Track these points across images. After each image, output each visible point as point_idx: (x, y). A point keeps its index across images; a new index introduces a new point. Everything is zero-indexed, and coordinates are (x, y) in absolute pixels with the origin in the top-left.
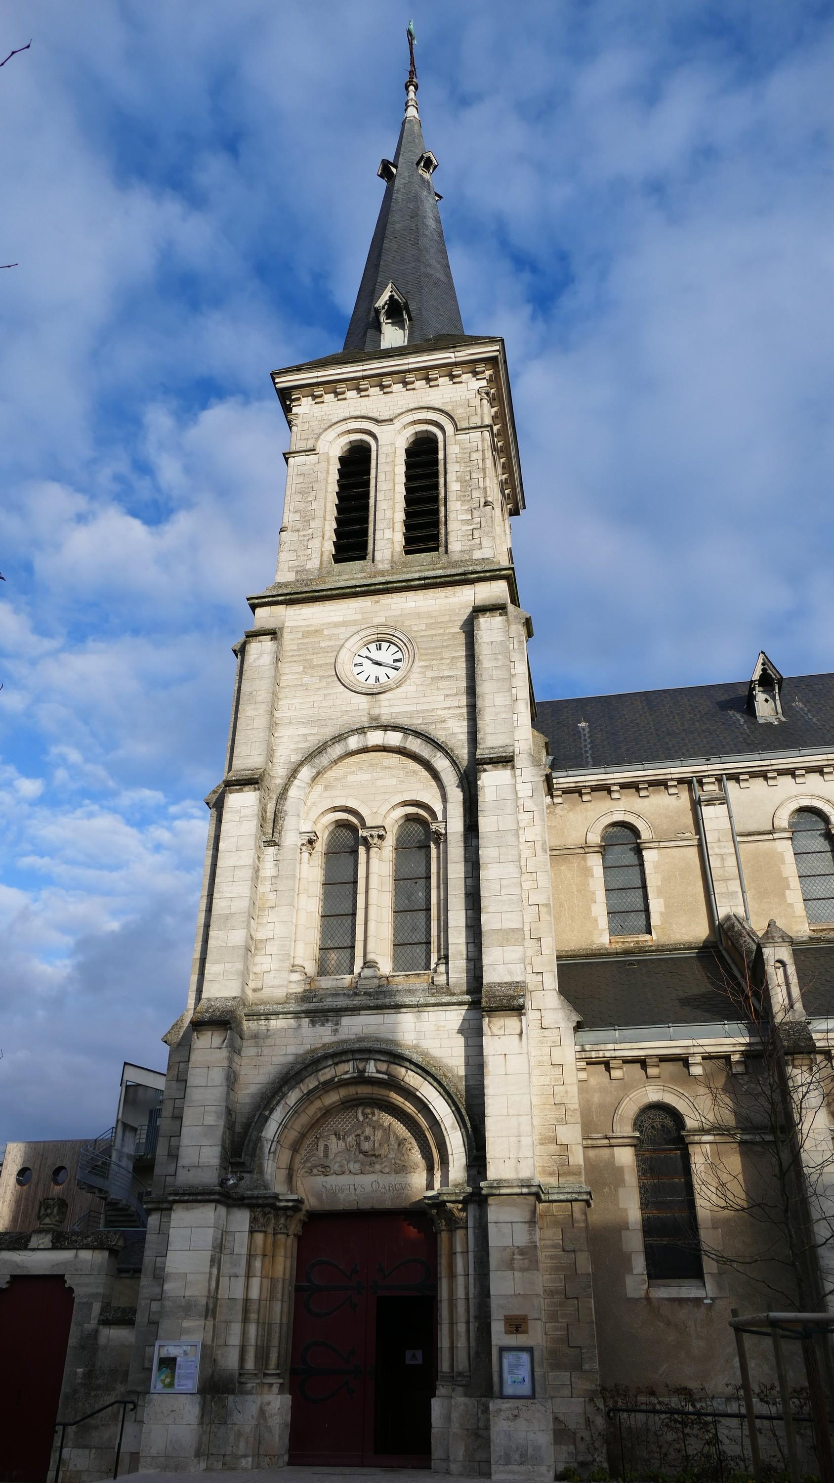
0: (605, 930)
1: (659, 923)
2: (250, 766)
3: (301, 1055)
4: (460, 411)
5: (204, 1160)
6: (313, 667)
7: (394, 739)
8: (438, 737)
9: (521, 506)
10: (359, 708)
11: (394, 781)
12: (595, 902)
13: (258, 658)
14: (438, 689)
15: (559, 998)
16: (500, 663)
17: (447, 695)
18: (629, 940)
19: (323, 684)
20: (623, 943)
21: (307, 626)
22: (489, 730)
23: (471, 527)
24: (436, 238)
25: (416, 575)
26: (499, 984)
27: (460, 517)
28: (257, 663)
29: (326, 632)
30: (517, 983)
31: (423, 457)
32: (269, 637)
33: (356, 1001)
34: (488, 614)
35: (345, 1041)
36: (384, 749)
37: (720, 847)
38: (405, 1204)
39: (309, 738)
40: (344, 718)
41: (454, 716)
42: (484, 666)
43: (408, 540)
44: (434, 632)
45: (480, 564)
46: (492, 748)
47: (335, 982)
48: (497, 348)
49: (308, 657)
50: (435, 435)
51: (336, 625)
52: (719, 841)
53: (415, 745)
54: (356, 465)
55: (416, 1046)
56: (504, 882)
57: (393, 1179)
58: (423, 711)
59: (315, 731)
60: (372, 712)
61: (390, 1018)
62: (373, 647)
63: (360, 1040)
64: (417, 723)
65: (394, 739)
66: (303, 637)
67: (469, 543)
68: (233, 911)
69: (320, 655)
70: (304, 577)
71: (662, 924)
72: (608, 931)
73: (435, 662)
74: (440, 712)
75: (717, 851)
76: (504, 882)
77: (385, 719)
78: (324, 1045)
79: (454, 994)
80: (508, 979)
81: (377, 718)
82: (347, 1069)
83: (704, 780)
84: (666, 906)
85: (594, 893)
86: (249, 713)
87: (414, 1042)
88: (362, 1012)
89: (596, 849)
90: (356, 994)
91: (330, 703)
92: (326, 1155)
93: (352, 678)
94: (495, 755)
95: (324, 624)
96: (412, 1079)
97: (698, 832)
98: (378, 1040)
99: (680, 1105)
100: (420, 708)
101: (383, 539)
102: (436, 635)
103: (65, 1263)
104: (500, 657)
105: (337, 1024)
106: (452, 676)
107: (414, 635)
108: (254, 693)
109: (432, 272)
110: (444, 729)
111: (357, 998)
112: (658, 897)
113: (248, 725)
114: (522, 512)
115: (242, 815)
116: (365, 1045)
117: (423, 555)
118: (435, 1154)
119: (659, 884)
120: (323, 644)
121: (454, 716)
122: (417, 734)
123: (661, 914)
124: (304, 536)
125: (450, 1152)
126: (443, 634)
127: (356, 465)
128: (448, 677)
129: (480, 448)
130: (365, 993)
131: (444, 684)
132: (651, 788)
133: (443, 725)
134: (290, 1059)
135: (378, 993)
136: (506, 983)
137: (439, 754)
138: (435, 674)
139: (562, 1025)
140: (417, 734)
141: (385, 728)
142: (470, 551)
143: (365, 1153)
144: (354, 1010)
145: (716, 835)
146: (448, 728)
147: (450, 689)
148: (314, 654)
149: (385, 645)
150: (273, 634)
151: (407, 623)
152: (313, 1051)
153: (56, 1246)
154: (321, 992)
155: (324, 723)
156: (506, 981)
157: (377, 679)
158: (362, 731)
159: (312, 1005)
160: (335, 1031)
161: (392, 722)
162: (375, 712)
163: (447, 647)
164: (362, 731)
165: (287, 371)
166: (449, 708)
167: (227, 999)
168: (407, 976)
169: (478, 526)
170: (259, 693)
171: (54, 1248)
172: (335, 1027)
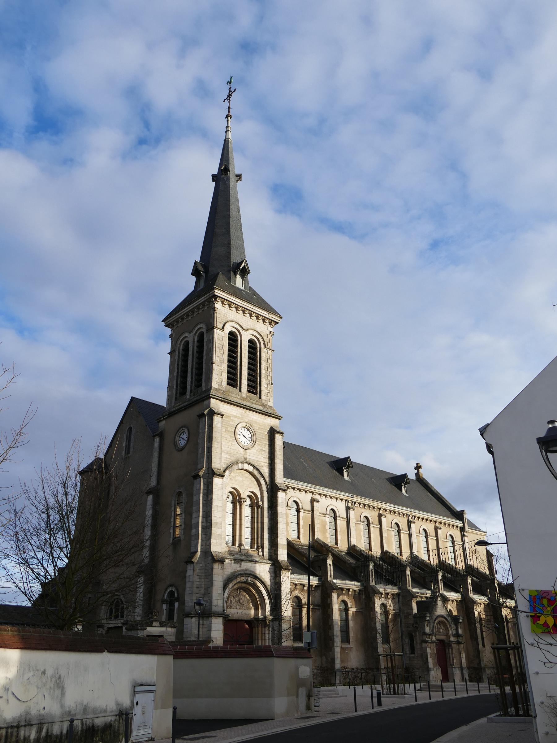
6: (228, 431)
7: (251, 469)
29: (232, 418)
35: (243, 570)
36: (246, 470)
38: (249, 619)
50: (237, 335)
51: (235, 416)
53: (256, 473)
57: (246, 611)
61: (253, 565)
62: (243, 429)
63: (246, 570)
64: (256, 464)
65: (251, 469)
81: (245, 459)
82: (243, 579)
92: (231, 603)
96: (259, 584)
97: (409, 530)
98: (251, 571)
99: (301, 597)
103: (163, 632)
116: (247, 572)
118: (258, 604)
121: (265, 466)
122: (257, 469)
125: (15, 604)
131: (263, 452)
134: (229, 573)
140: (257, 469)
143: (241, 603)
149: (246, 430)
153: (161, 626)
160: (240, 566)
162: (246, 456)
164: (243, 462)
171: (160, 627)
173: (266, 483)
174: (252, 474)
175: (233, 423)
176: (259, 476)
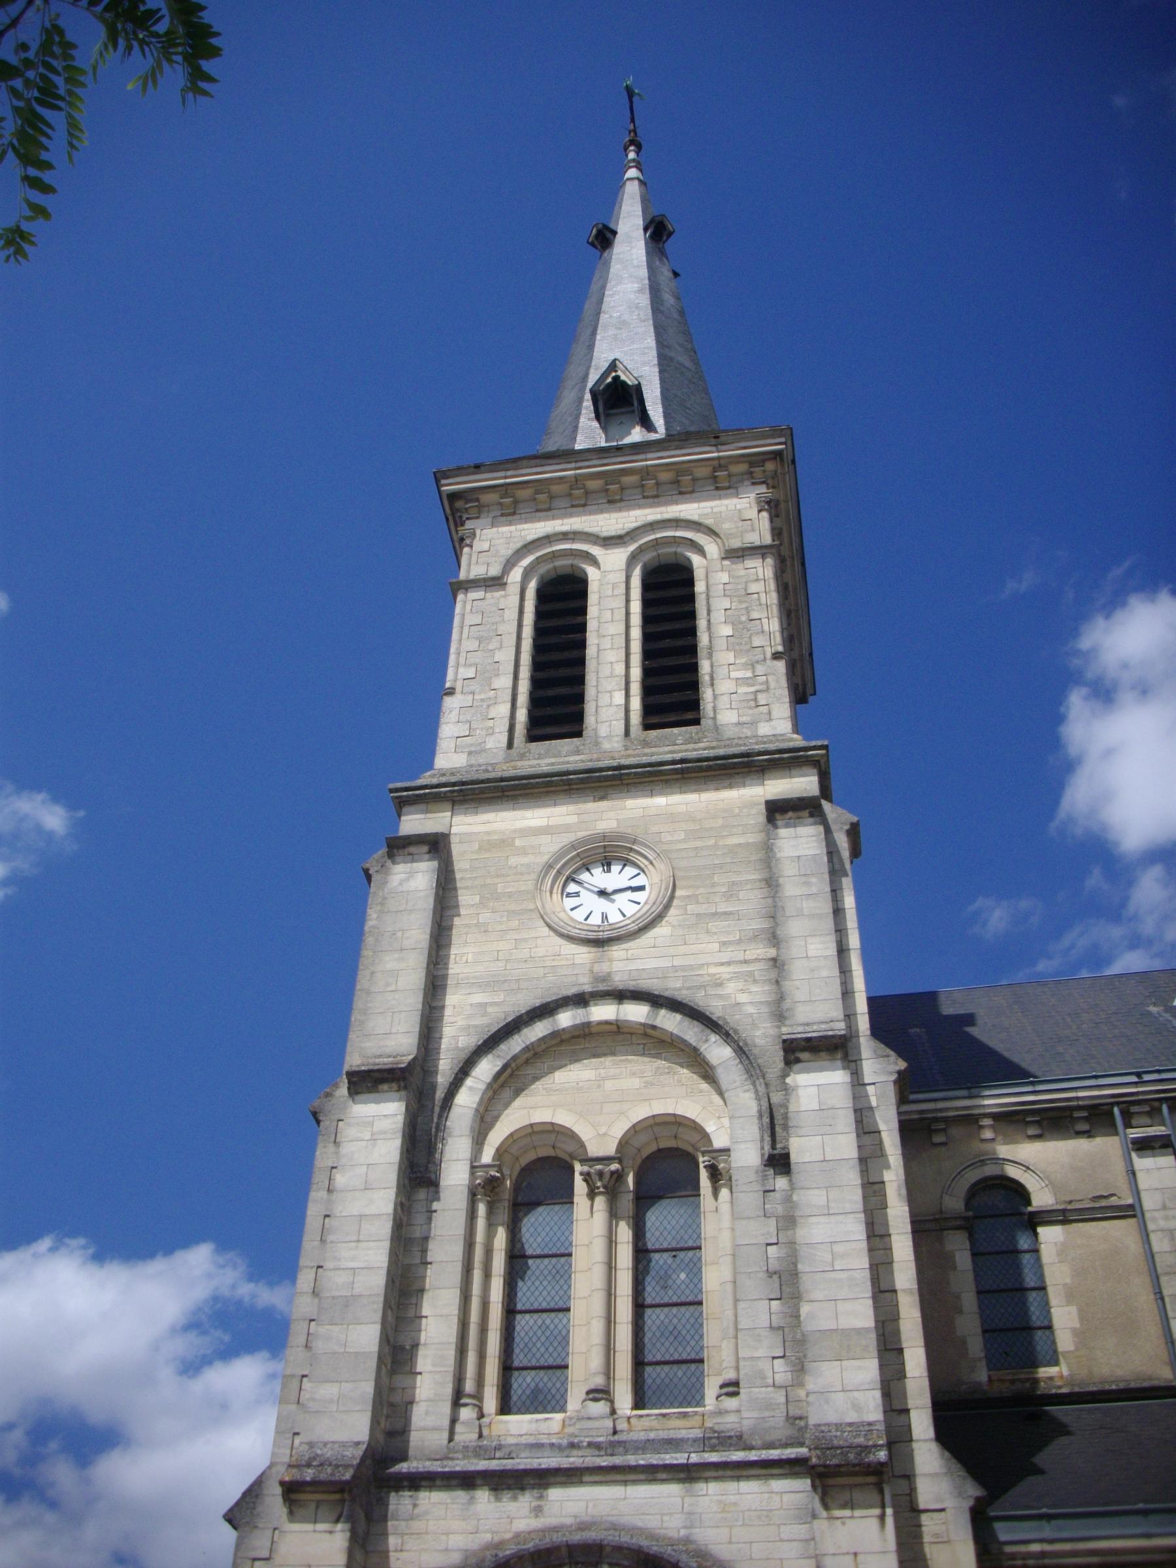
0: (980, 1359)
1: (1072, 1348)
2: (388, 1051)
3: (474, 1553)
4: (726, 526)
5: (846, 1322)
7: (636, 1012)
8: (712, 1009)
9: (809, 691)
10: (576, 966)
11: (636, 1082)
12: (961, 1312)
13: (407, 879)
14: (708, 932)
15: (942, 1455)
16: (814, 890)
17: (724, 943)
18: (1022, 1376)
19: (515, 924)
20: (1013, 1382)
21: (488, 833)
22: (800, 995)
23: (752, 689)
24: (676, 315)
25: (668, 757)
26: (838, 1426)
27: (734, 675)
28: (405, 887)
29: (518, 843)
30: (870, 1424)
31: (669, 596)
32: (425, 848)
33: (574, 1460)
34: (790, 814)
35: (555, 1529)
37: (1166, 1218)
39: (490, 1010)
40: (551, 978)
41: (736, 976)
42: (788, 894)
43: (649, 710)
44: (699, 844)
45: (771, 742)
46: (808, 1024)
47: (534, 1426)
48: (783, 440)
49: (489, 881)
52: (1164, 1207)
54: (561, 605)
55: (687, 1541)
56: (838, 1248)
58: (683, 968)
59: (500, 997)
60: (596, 968)
63: (583, 1526)
64: (673, 987)
66: (480, 848)
67: (751, 712)
68: (356, 1291)
69: (509, 879)
70: (481, 761)
71: (1077, 1349)
72: (984, 1363)
73: (702, 890)
74: (713, 970)
75: (1162, 1224)
76: (838, 1248)
77: (620, 980)
78: (517, 1535)
79: (751, 1448)
80: (852, 1417)
83: (1134, 1109)
84: (1082, 1318)
85: (958, 1297)
86: (390, 966)
87: (683, 1532)
88: (586, 1478)
89: (958, 1223)
90: (572, 1446)
91: (525, 954)
93: (562, 915)
94: (815, 1035)
95: (515, 831)
98: (615, 1527)
100: (677, 962)
101: (610, 705)
102: (702, 848)
104: (814, 880)
105: (541, 1497)
106: (731, 913)
107: (665, 847)
108: (399, 934)
109: (672, 354)
110: (720, 997)
111: (575, 1452)
112: (1069, 1303)
113: (387, 985)
114: (811, 699)
115: (375, 1129)
117: (676, 730)
119: (1068, 1280)
120: (513, 861)
121: (736, 976)
123: (1074, 1331)
124: (482, 700)
126: (715, 847)
127: (561, 605)
128: (725, 913)
129: (761, 576)
130: (590, 1444)
131: (713, 926)
132: (1045, 1123)
133: (720, 991)
135: (613, 1444)
136: (850, 1424)
137: (714, 1038)
138: (702, 909)
139: (949, 1503)
141: (621, 996)
142: (754, 724)
144: (571, 1476)
145: (1158, 1196)
146: (728, 997)
147: (729, 933)
148: (498, 876)
150: (437, 845)
151: (654, 829)
152: (499, 1545)
154: (511, 1441)
155: (514, 986)
156: (848, 1420)
157: (605, 917)
158: (581, 1000)
159: (495, 1462)
160: (538, 1511)
161: (632, 985)
162: (604, 968)
163: (721, 866)
164: (581, 1000)
165: (460, 471)
166: (729, 963)
167: (344, 1445)
168: (664, 1415)
169: (764, 687)
170: (407, 934)
172: (535, 1504)
173: (742, 1051)
174: (650, 1042)
175: (525, 860)
176: (689, 1031)
